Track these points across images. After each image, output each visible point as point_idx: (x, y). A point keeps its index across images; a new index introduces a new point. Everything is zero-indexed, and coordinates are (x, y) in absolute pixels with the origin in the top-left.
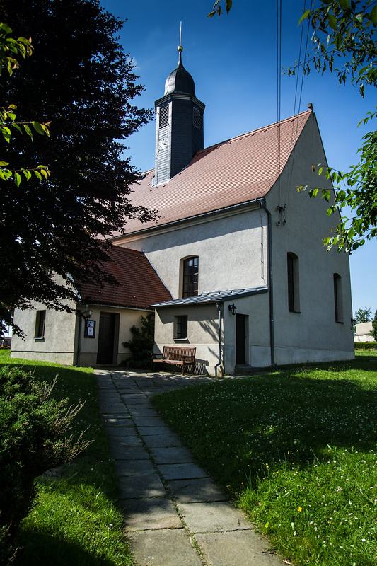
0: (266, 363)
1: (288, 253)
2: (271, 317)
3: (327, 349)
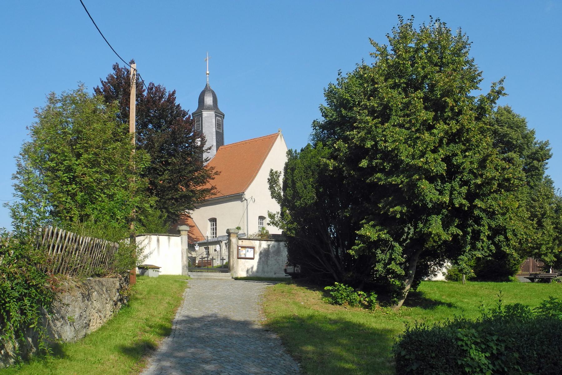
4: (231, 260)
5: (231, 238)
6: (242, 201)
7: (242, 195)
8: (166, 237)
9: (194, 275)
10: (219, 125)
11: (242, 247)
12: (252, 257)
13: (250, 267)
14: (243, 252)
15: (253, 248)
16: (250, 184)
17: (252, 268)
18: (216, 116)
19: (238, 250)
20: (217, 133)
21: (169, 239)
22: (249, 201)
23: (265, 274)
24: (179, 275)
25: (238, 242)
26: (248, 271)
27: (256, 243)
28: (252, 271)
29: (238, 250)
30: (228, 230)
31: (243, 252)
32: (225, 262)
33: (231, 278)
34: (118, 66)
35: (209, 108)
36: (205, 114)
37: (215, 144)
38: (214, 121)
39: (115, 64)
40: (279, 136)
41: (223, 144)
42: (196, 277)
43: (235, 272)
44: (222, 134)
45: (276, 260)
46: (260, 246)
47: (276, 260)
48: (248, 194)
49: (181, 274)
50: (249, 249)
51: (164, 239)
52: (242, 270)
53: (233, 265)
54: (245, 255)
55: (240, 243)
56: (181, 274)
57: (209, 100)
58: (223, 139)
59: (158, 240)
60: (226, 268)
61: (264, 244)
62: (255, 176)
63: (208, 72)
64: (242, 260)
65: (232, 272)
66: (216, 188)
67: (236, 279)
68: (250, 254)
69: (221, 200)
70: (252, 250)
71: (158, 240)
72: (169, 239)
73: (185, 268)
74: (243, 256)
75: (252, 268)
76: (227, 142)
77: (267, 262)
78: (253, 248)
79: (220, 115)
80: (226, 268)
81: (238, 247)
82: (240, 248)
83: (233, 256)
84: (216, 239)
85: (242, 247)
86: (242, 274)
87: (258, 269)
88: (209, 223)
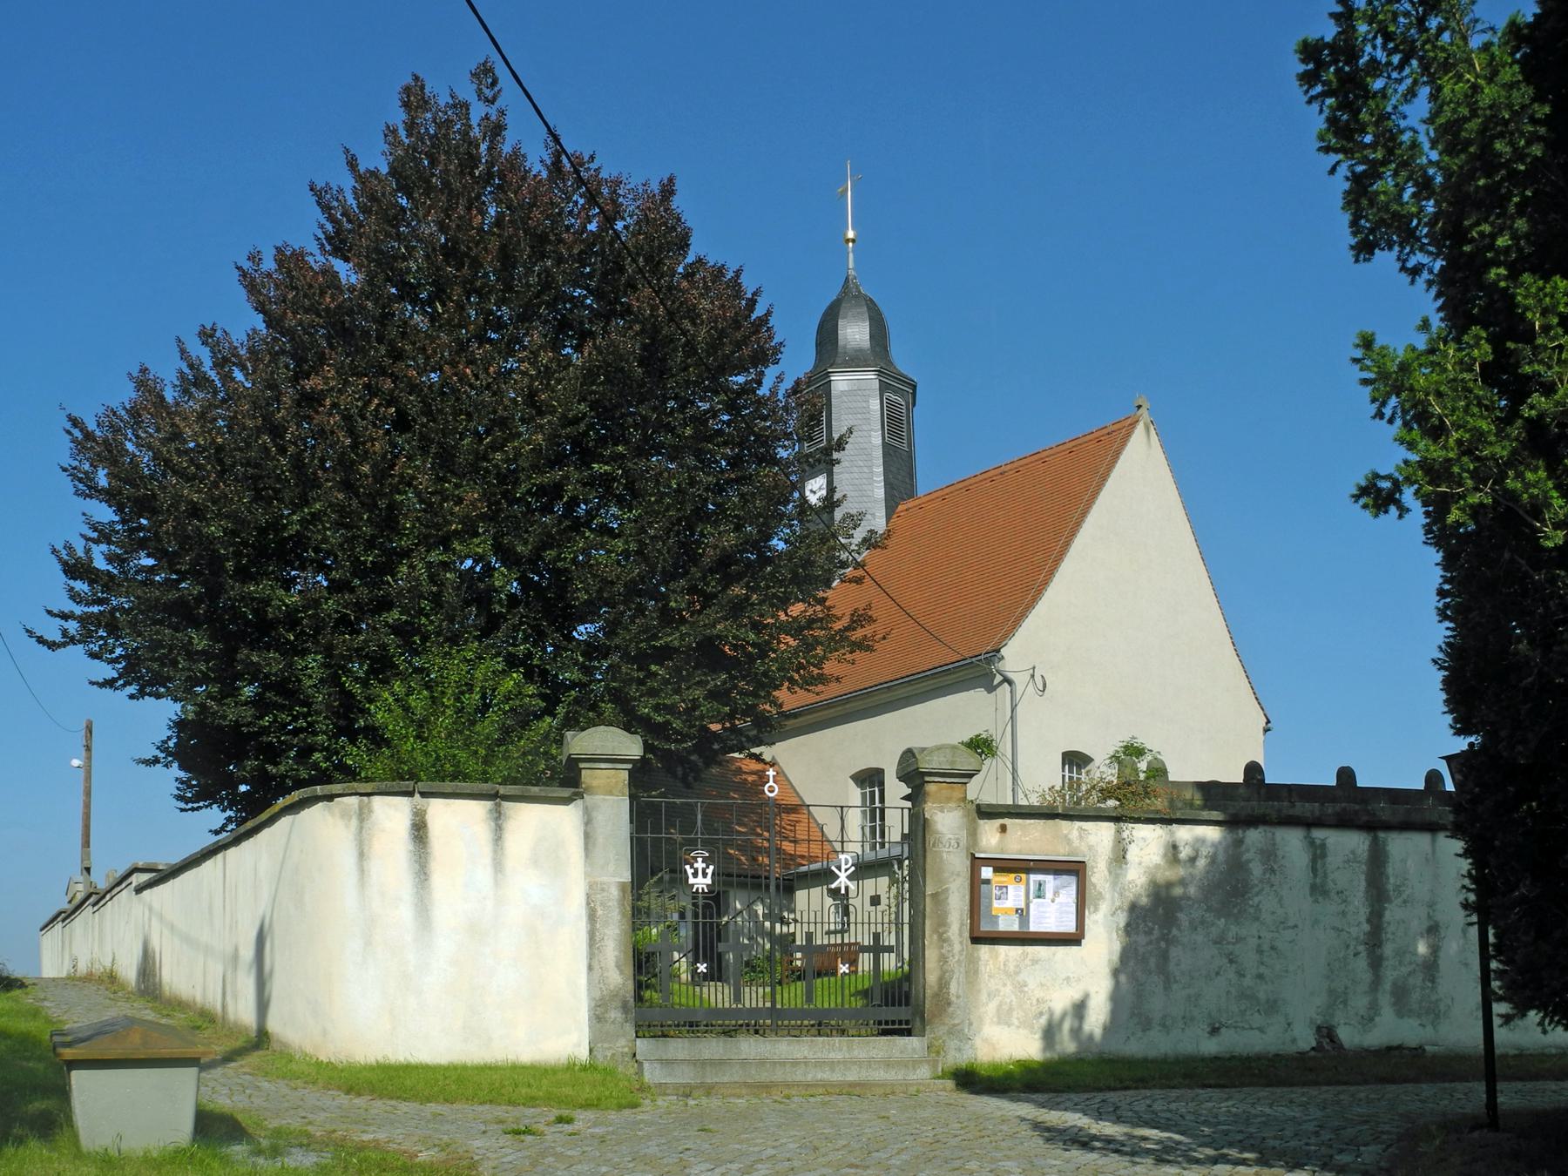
4: (931, 956)
5: (931, 810)
6: (991, 689)
7: (989, 661)
8: (476, 810)
9: (668, 1062)
10: (896, 425)
11: (1005, 866)
12: (1070, 927)
13: (1061, 1001)
14: (1008, 899)
15: (1075, 869)
16: (1023, 615)
17: (1080, 1009)
18: (884, 387)
19: (976, 883)
20: (889, 451)
21: (498, 818)
22: (1019, 689)
23: (1155, 1034)
24: (571, 1067)
25: (973, 834)
26: (1049, 1034)
27: (1096, 839)
28: (1076, 1032)
29: (976, 883)
30: (909, 754)
31: (1008, 899)
32: (889, 962)
33: (924, 1072)
34: (422, 87)
35: (856, 361)
36: (841, 382)
37: (880, 492)
38: (875, 404)
39: (409, 80)
40: (1140, 427)
41: (911, 494)
42: (685, 1076)
43: (955, 1031)
44: (910, 457)
45: (1218, 942)
46: (1120, 856)
47: (1218, 942)
48: (1015, 655)
49: (583, 1054)
50: (1049, 880)
51: (458, 820)
52: (1003, 1017)
53: (943, 984)
54: (1023, 914)
55: (990, 838)
56: (583, 1054)
57: (855, 333)
58: (911, 475)
59: (419, 830)
60: (898, 1006)
61: (1148, 845)
62: (1045, 584)
63: (851, 234)
64: (1003, 950)
65: (937, 1031)
66: (871, 620)
67: (970, 1080)
68: (1053, 908)
69: (901, 692)
70: (1070, 883)
71: (419, 830)
72: (498, 818)
73: (615, 1014)
74: (1008, 924)
75: (1080, 1009)
76: (927, 480)
77: (1164, 957)
78: (1075, 869)
79: (899, 391)
80: (898, 1006)
81: (976, 862)
82: (987, 872)
83: (942, 923)
84: (883, 854)
85: (1005, 866)
86: (1006, 1039)
87: (1114, 1013)
88: (855, 795)
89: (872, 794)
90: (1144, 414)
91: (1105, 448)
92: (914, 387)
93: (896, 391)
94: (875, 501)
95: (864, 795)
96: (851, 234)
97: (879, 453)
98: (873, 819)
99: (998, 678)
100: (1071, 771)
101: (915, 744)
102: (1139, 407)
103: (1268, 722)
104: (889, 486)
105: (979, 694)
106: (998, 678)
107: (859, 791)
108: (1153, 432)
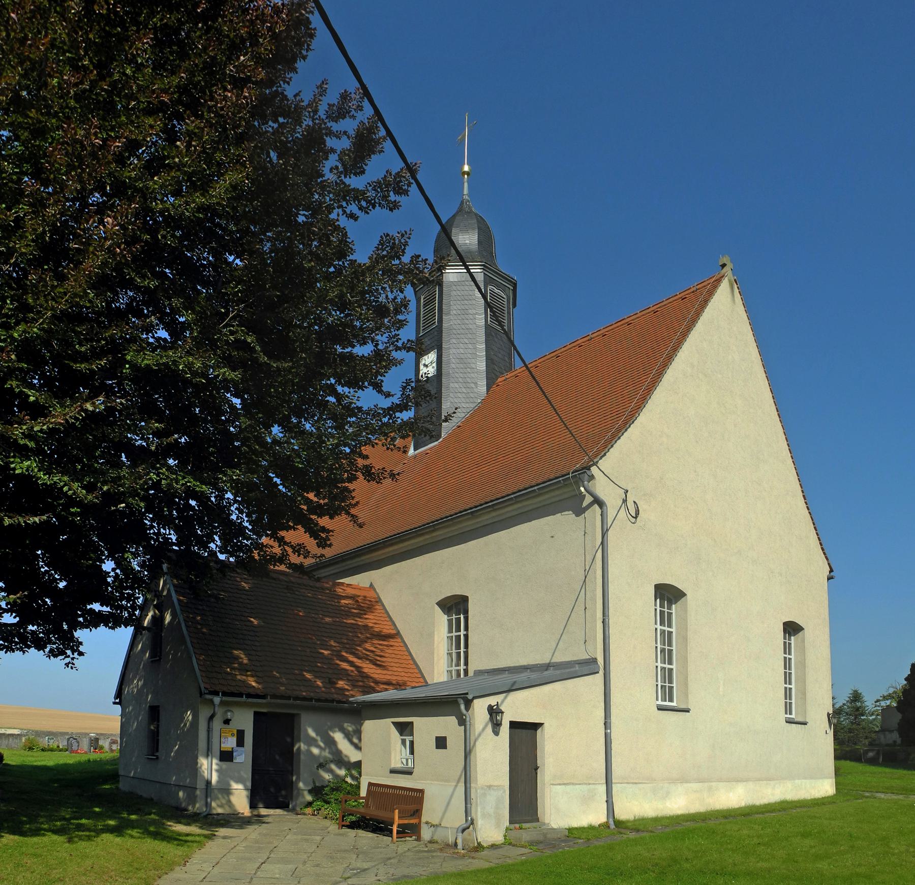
0: (596, 816)
1: (656, 586)
2: (607, 725)
3: (759, 780)
6: (579, 511)
7: (578, 481)
22: (611, 513)
36: (453, 274)
37: (482, 366)
40: (724, 285)
48: (612, 472)
62: (670, 358)
63: (466, 168)
88: (442, 620)
89: (458, 620)
90: (727, 270)
91: (694, 303)
92: (515, 285)
93: (498, 286)
94: (478, 372)
95: (450, 621)
96: (466, 168)
97: (482, 332)
98: (458, 646)
99: (588, 499)
100: (662, 606)
101: (689, 595)
102: (724, 266)
103: (831, 571)
104: (490, 361)
105: (567, 517)
106: (588, 499)
107: (445, 618)
108: (736, 291)
